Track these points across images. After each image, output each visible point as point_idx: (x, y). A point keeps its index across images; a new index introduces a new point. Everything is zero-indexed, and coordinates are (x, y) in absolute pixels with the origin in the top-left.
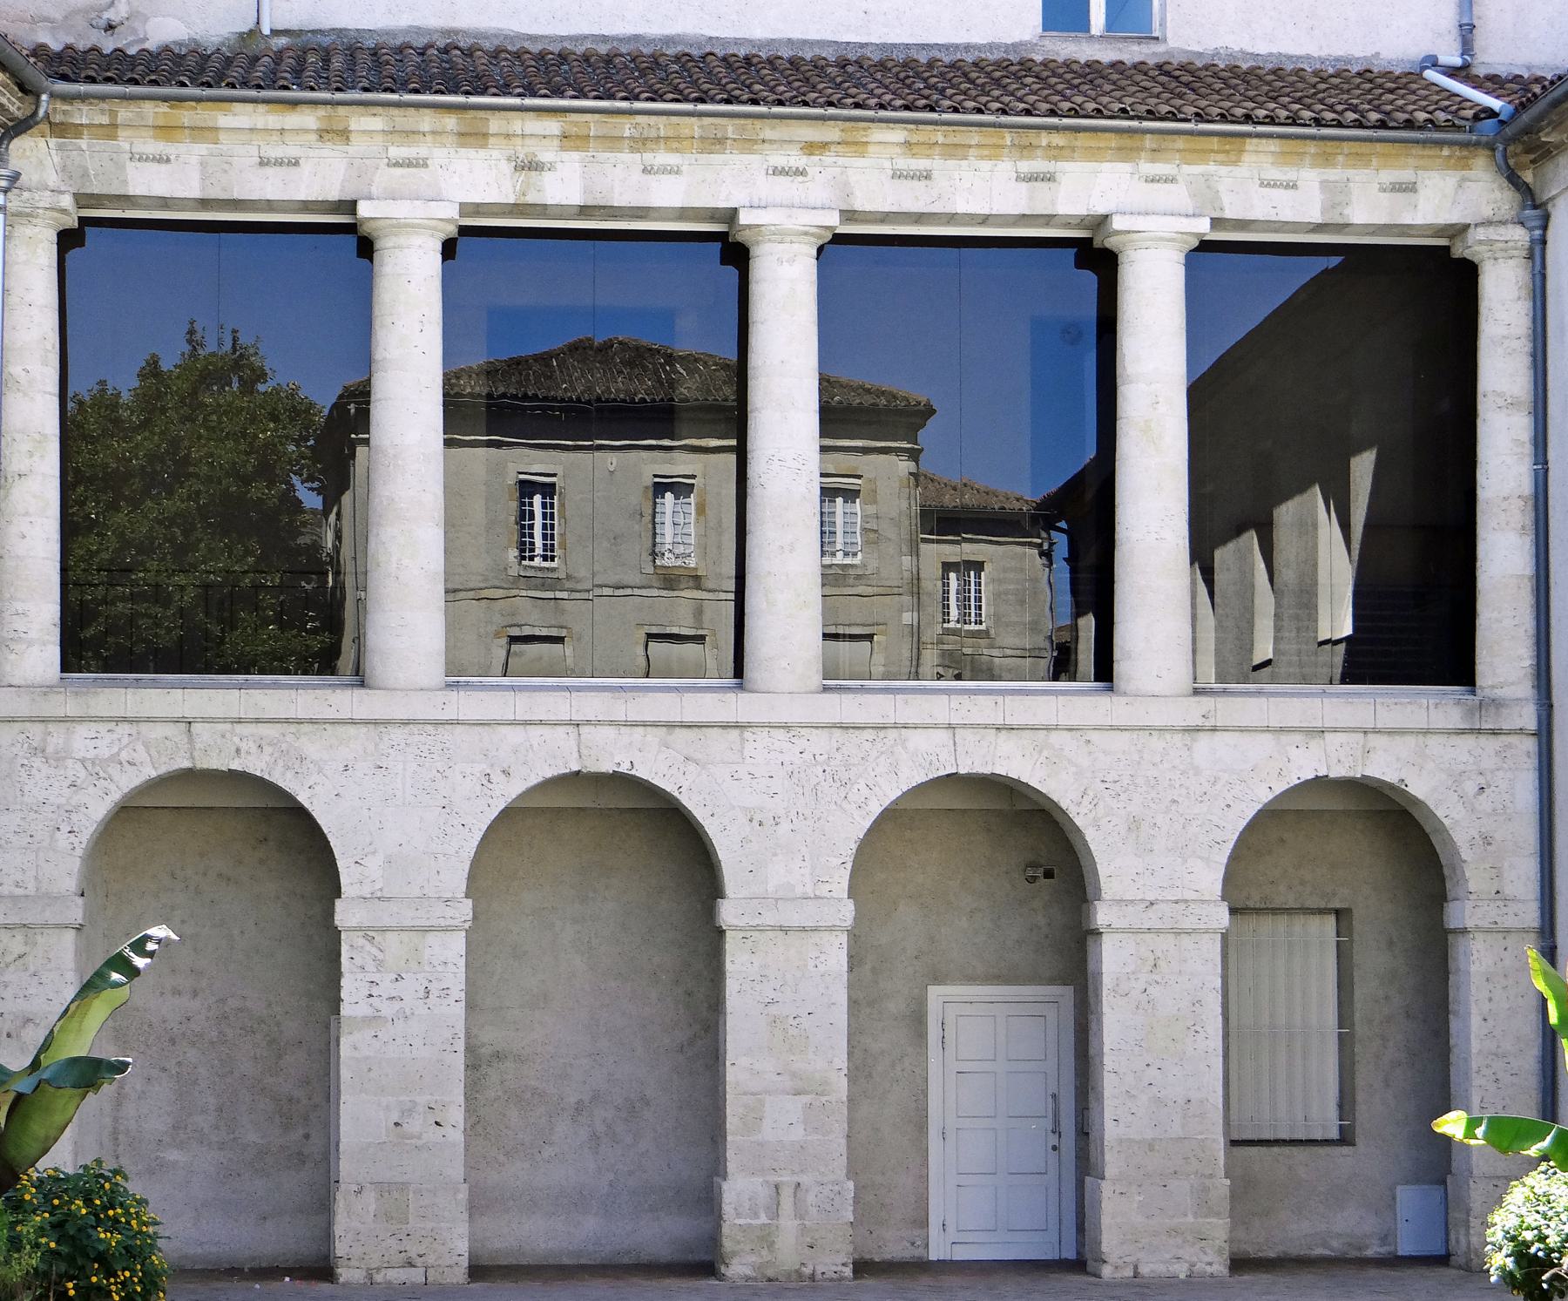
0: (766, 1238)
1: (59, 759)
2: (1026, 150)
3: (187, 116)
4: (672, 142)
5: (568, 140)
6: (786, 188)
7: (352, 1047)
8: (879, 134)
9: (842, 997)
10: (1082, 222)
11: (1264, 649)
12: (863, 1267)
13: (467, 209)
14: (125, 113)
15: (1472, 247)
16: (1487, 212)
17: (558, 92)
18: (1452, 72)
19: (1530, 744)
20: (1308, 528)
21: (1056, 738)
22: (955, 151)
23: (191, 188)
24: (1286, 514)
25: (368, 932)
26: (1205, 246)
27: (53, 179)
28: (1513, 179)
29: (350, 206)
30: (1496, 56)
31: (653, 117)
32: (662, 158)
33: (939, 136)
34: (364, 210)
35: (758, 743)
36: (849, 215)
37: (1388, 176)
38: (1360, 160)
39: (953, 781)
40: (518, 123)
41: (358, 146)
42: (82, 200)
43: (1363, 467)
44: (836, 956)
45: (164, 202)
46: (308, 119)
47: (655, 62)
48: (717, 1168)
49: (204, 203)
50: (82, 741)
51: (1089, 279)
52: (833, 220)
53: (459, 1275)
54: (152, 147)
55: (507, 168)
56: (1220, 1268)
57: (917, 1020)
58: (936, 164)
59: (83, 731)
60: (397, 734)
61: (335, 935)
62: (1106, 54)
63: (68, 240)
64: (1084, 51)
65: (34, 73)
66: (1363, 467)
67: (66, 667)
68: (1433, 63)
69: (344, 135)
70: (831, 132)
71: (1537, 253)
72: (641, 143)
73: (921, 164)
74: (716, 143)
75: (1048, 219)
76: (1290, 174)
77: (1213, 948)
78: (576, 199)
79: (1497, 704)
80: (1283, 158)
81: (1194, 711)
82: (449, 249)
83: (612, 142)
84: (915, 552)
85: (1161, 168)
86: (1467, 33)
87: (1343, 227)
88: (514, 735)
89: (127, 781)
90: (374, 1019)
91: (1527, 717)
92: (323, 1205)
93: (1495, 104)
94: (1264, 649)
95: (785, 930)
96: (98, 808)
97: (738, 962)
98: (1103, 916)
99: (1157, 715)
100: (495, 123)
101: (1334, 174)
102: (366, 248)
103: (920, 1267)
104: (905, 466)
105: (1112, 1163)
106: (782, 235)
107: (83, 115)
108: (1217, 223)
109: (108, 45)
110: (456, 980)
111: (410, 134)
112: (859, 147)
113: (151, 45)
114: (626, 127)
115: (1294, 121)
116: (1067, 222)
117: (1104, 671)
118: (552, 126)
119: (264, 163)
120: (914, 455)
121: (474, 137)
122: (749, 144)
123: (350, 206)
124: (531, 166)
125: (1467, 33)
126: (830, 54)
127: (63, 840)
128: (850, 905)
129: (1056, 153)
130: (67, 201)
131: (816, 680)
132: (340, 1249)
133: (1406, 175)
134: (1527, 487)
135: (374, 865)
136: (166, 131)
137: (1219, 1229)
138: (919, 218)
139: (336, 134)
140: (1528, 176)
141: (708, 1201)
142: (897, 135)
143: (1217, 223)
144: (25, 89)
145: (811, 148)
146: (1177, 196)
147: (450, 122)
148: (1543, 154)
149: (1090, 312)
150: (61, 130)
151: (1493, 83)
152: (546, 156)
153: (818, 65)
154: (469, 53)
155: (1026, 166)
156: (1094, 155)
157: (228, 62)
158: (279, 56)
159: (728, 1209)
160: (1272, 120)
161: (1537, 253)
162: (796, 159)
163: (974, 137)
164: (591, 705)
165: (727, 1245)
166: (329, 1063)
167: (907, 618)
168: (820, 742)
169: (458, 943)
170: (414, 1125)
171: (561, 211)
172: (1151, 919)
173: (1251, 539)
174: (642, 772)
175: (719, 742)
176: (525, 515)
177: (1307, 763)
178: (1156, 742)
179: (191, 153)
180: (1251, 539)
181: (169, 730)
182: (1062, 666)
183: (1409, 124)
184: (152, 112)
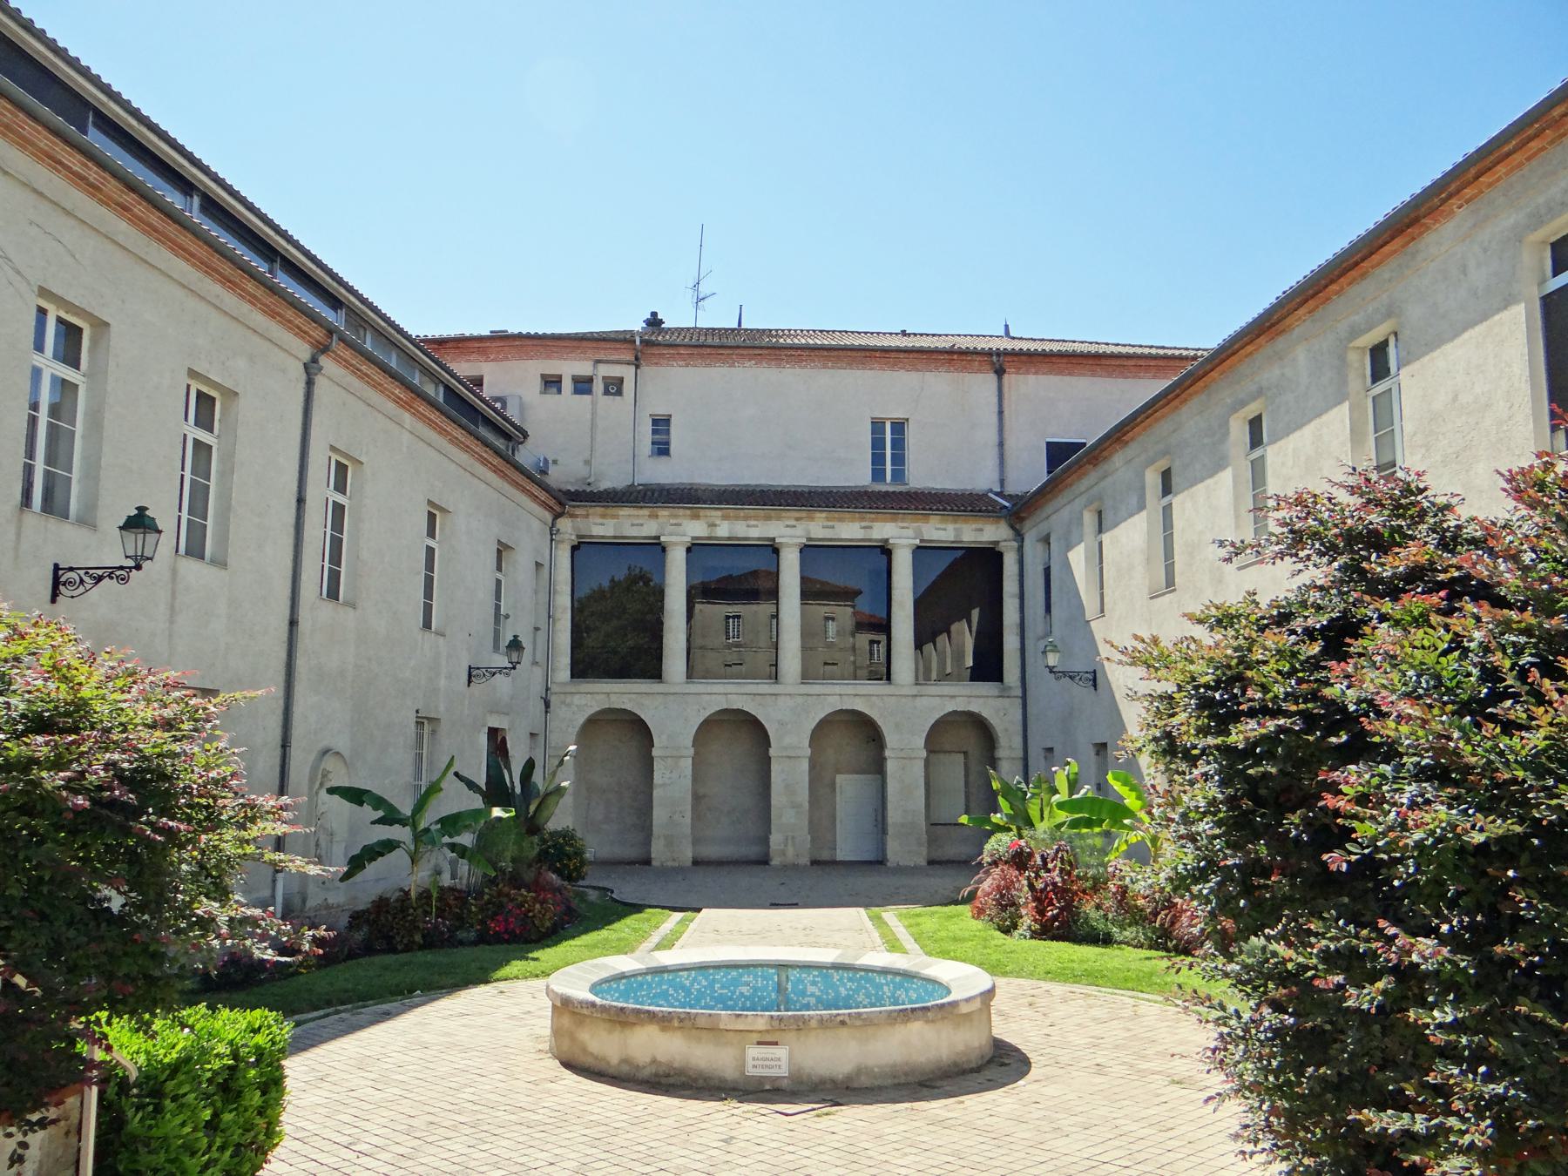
0: (783, 853)
1: (569, 705)
2: (863, 519)
3: (610, 511)
4: (756, 518)
5: (725, 518)
6: (789, 531)
7: (657, 793)
8: (818, 515)
9: (807, 779)
10: (881, 540)
11: (949, 670)
12: (815, 863)
13: (693, 538)
14: (591, 511)
15: (1002, 547)
16: (1005, 537)
17: (720, 503)
18: (997, 494)
19: (1020, 701)
20: (962, 633)
21: (874, 698)
22: (841, 520)
23: (610, 532)
24: (954, 627)
25: (662, 758)
26: (919, 547)
27: (570, 531)
28: (1012, 527)
29: (658, 538)
30: (1013, 488)
31: (750, 510)
32: (752, 522)
33: (836, 515)
34: (662, 539)
35: (781, 700)
36: (809, 539)
37: (974, 526)
38: (966, 522)
39: (841, 711)
40: (709, 513)
41: (661, 520)
42: (578, 536)
43: (975, 614)
44: (805, 765)
45: (603, 537)
46: (646, 512)
47: (753, 492)
48: (769, 831)
49: (615, 537)
50: (577, 700)
51: (884, 557)
52: (804, 541)
53: (689, 863)
54: (600, 521)
55: (705, 526)
56: (924, 863)
57: (833, 786)
58: (837, 524)
59: (577, 696)
60: (671, 697)
61: (652, 759)
62: (891, 489)
63: (574, 549)
64: (883, 488)
65: (563, 499)
66: (975, 614)
67: (573, 676)
68: (991, 491)
69: (657, 516)
70: (804, 514)
71: (1020, 550)
72: (746, 518)
73: (830, 524)
74: (768, 518)
75: (870, 540)
76: (943, 526)
77: (922, 763)
78: (726, 535)
79: (1010, 688)
80: (942, 522)
81: (915, 690)
82: (689, 550)
83: (737, 518)
84: (854, 636)
85: (905, 525)
86: (1002, 482)
87: (961, 542)
88: (708, 697)
89: (592, 711)
90: (663, 785)
91: (1019, 692)
92: (647, 841)
93: (1007, 504)
94: (949, 670)
95: (789, 757)
96: (581, 720)
97: (775, 767)
98: (887, 753)
99: (905, 691)
100: (702, 513)
101: (957, 526)
102: (664, 550)
103: (834, 863)
104: (850, 610)
105: (891, 830)
106: (788, 545)
107: (578, 511)
108: (921, 541)
109: (588, 489)
110: (689, 771)
111: (676, 516)
112: (812, 519)
113: (601, 489)
114: (742, 513)
115: (944, 510)
116: (876, 540)
117: (889, 678)
118: (719, 513)
119: (633, 525)
120: (853, 607)
121: (696, 517)
122: (779, 518)
123: (658, 538)
124: (713, 525)
125: (1002, 482)
126: (806, 490)
127: (570, 730)
128: (809, 751)
129: (873, 520)
130: (573, 537)
131: (799, 681)
132: (653, 856)
133: (980, 526)
134: (1018, 621)
135: (664, 737)
136: (603, 516)
137: (924, 851)
138: (831, 540)
139: (654, 516)
140: (1018, 527)
141: (765, 840)
142: (824, 515)
143: (921, 541)
144: (562, 504)
145: (797, 519)
146: (910, 532)
147: (688, 512)
148: (1022, 520)
149: (885, 568)
150: (572, 516)
151: (1009, 498)
152: (718, 522)
153: (802, 493)
154: (696, 490)
155: (863, 524)
156: (885, 521)
157: (624, 494)
158: (639, 492)
159: (771, 844)
160: (938, 510)
161: (1020, 550)
162: (793, 522)
163: (847, 515)
164: (731, 688)
165: (771, 854)
166: (913, 1010)
167: (852, 658)
168: (800, 700)
169: (690, 761)
170: (676, 817)
171: (722, 539)
172: (902, 755)
173: (945, 635)
174: (745, 709)
175: (769, 700)
176: (420, 737)
177: (723, 704)
178: (904, 700)
179: (611, 522)
180: (945, 635)
181: (603, 696)
182: (874, 676)
183: (980, 511)
184: (600, 510)
